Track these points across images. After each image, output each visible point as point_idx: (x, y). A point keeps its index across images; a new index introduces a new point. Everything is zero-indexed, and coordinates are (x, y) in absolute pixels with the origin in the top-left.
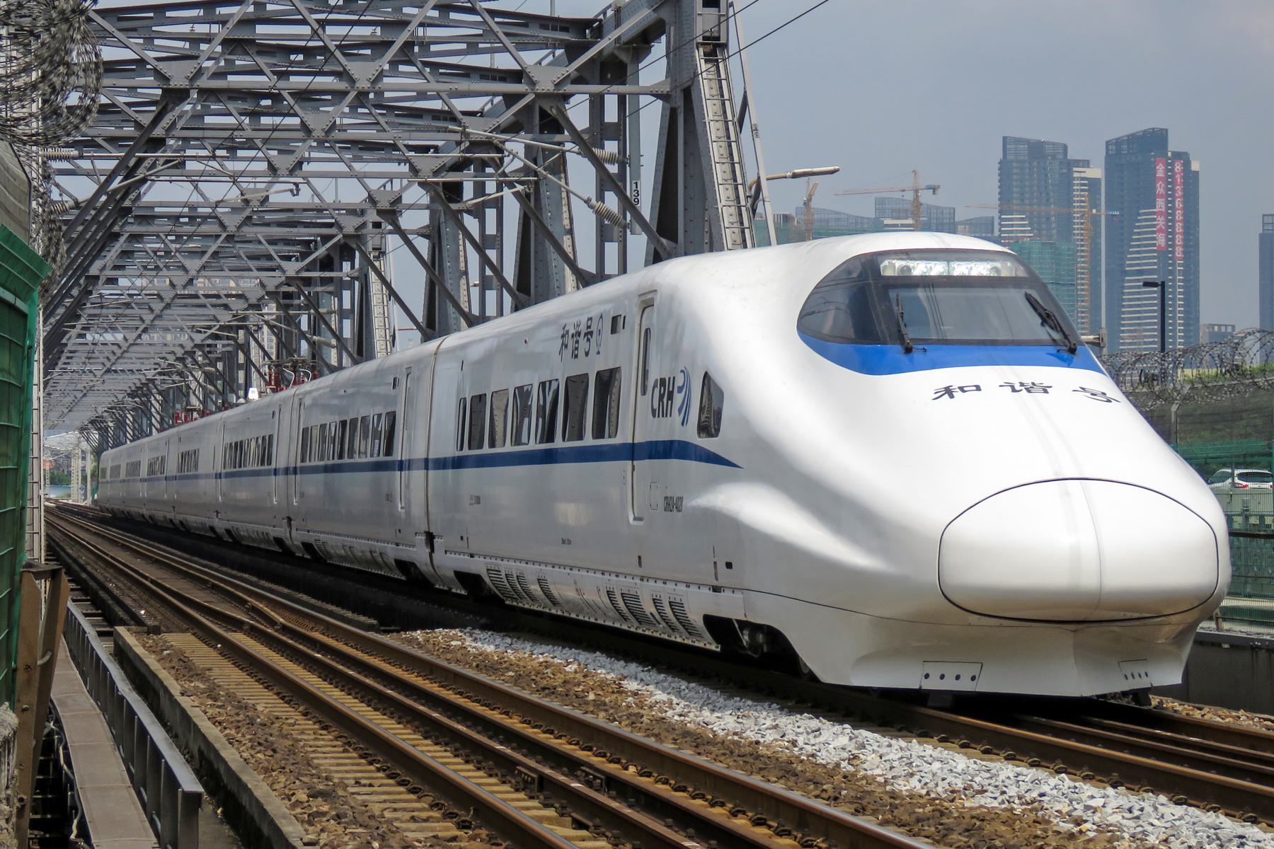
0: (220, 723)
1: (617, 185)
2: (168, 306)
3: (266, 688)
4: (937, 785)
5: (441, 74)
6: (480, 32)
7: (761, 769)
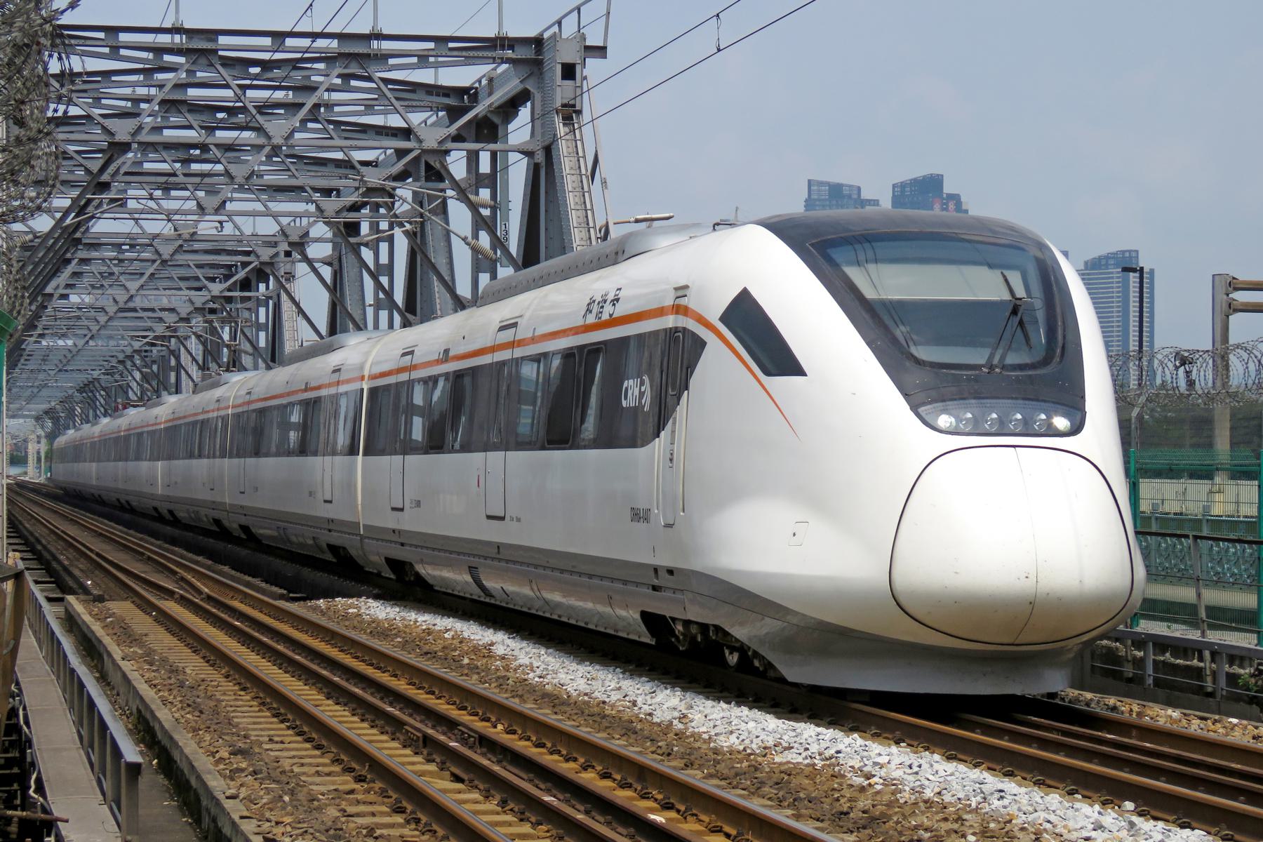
0: (155, 686)
1: (489, 227)
2: (111, 319)
3: (194, 652)
4: (752, 742)
5: (343, 130)
6: (376, 96)
7: (607, 728)
